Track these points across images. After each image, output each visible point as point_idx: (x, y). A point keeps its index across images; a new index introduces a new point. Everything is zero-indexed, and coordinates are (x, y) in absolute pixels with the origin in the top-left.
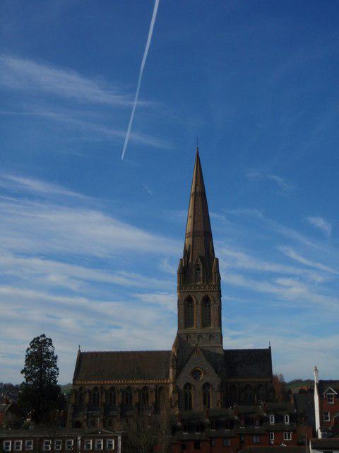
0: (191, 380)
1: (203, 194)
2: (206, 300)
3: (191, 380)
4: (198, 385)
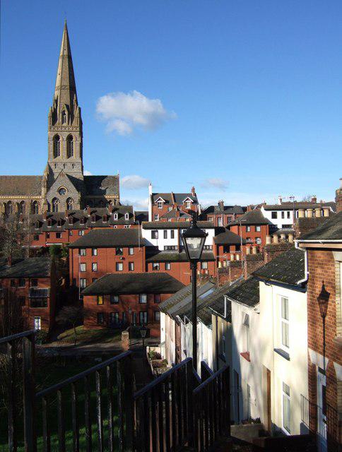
0: (58, 196)
1: (70, 57)
3: (58, 196)
4: (63, 199)
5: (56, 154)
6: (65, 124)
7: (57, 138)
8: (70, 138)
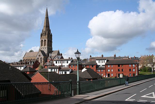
1: (47, 18)
4: (40, 58)
5: (42, 45)
6: (44, 37)
7: (42, 41)
8: (45, 40)
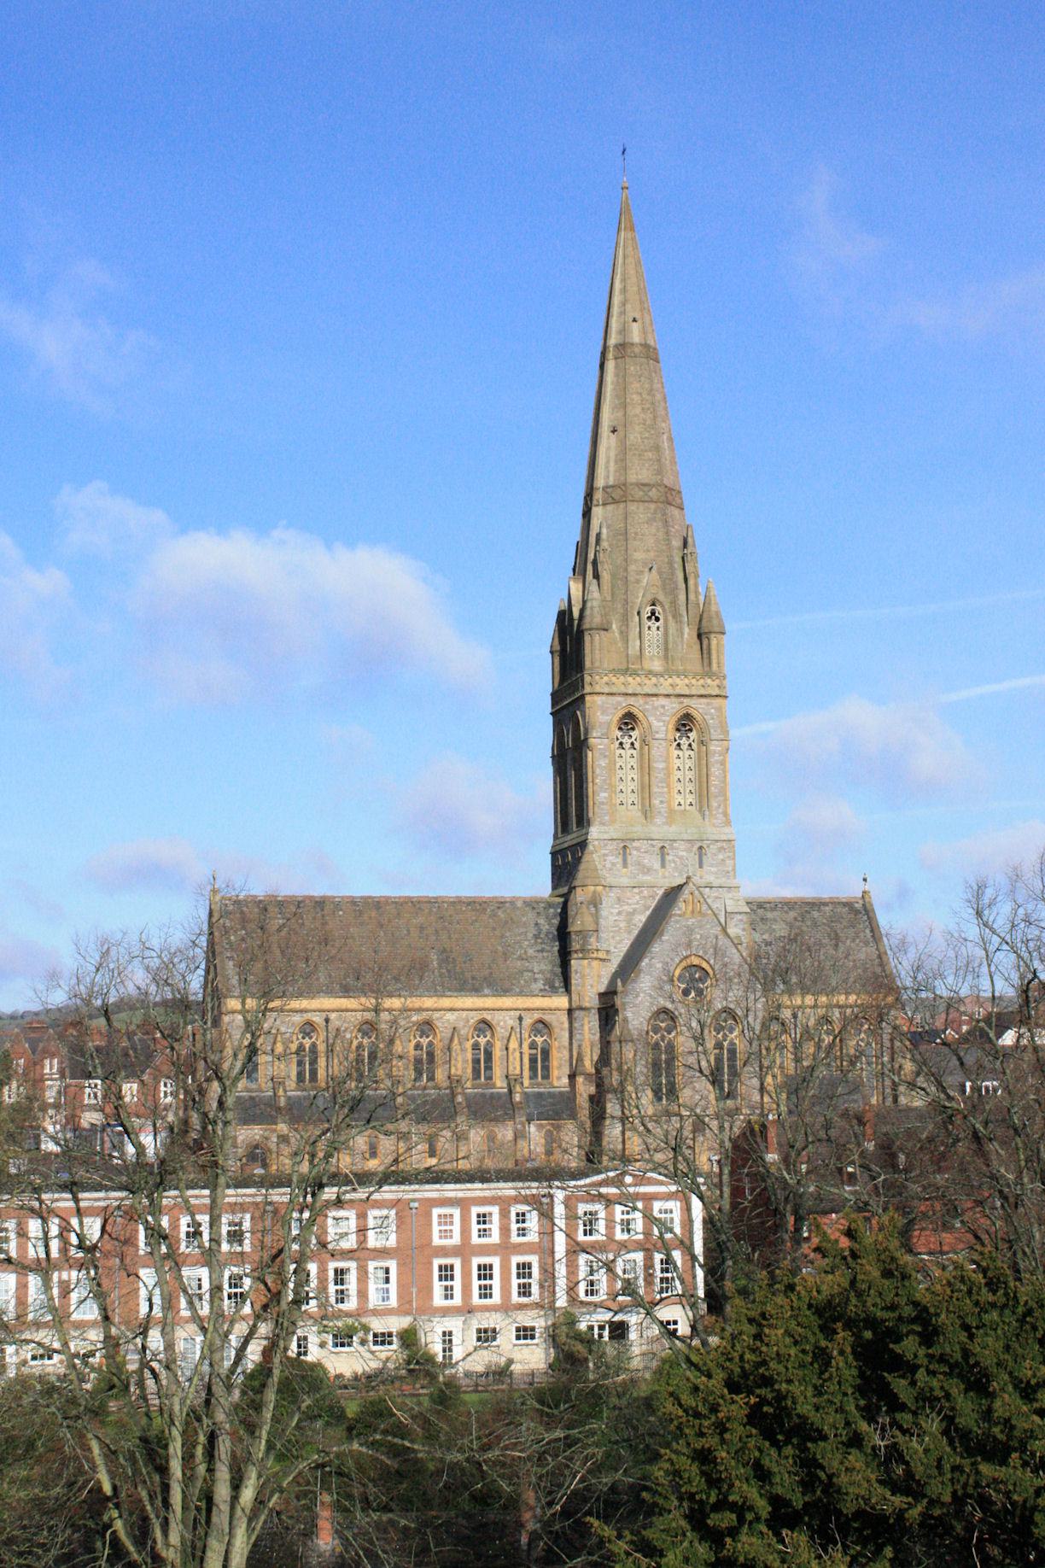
2: (685, 723)
